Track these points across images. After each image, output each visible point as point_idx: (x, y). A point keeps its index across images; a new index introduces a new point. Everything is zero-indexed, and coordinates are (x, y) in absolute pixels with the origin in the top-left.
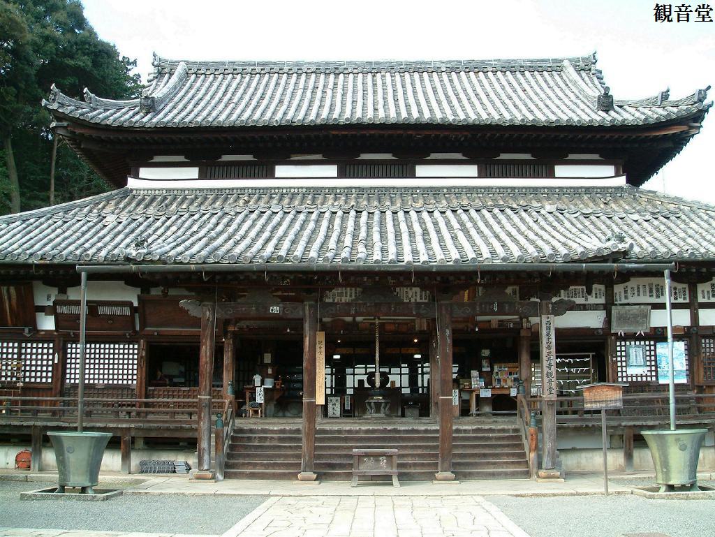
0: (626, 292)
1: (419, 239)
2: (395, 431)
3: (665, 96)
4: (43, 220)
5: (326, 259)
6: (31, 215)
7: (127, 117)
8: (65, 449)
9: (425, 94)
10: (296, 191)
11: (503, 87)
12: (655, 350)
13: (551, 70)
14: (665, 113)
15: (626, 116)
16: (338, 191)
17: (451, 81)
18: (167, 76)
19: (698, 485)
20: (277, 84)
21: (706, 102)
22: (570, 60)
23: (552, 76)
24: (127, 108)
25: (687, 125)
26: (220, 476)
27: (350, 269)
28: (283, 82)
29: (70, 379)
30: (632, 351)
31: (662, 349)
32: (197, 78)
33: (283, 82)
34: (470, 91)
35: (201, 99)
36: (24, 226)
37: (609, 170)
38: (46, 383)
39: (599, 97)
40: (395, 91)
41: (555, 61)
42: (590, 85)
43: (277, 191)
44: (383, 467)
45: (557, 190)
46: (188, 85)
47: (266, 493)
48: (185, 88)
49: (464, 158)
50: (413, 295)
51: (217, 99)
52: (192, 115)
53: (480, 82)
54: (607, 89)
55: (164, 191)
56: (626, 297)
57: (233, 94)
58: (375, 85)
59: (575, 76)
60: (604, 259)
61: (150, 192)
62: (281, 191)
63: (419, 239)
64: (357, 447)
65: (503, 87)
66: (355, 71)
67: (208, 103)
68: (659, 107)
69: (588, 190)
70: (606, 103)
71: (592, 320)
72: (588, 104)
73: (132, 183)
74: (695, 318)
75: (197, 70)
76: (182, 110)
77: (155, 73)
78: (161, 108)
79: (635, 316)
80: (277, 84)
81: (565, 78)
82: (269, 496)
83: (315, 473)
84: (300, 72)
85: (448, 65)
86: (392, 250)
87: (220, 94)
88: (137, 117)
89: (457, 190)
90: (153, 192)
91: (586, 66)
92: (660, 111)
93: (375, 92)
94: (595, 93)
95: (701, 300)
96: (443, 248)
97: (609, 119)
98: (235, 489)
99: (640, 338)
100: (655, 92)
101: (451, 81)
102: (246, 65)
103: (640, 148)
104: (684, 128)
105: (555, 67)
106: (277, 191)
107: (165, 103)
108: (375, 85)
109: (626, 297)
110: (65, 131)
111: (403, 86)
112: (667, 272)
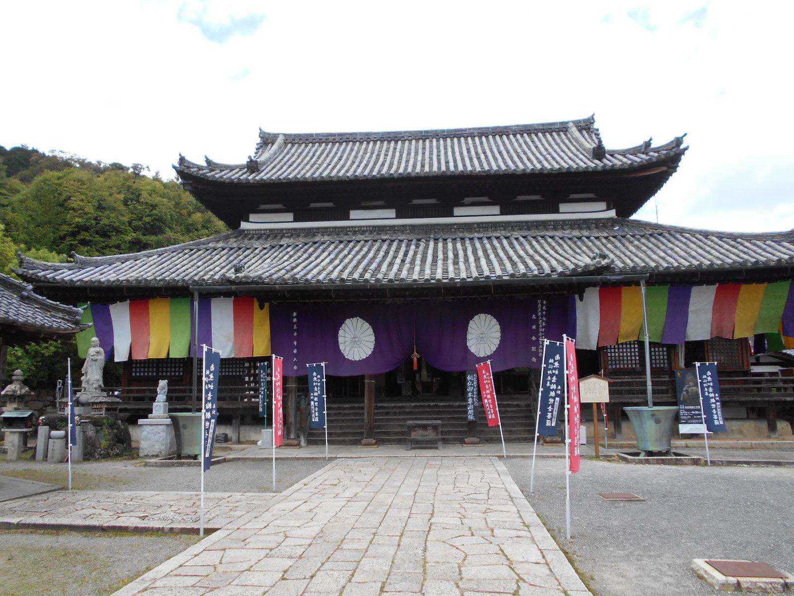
1: (450, 262)
2: (436, 406)
3: (648, 144)
4: (174, 254)
5: (378, 280)
6: (166, 250)
7: (237, 176)
8: (181, 426)
9: (461, 153)
10: (365, 229)
11: (520, 146)
13: (558, 131)
14: (648, 158)
15: (616, 162)
16: (396, 228)
17: (481, 143)
18: (270, 145)
19: (673, 451)
20: (352, 150)
21: (682, 147)
22: (574, 122)
23: (559, 135)
24: (238, 170)
26: (303, 443)
27: (394, 287)
28: (356, 148)
29: (136, 372)
32: (293, 146)
33: (356, 148)
34: (495, 150)
35: (294, 162)
36: (159, 258)
37: (603, 205)
38: (179, 376)
39: (594, 148)
40: (439, 152)
42: (589, 140)
43: (351, 229)
45: (561, 223)
46: (285, 152)
47: (334, 456)
48: (283, 154)
49: (490, 200)
51: (306, 161)
52: (286, 174)
53: (503, 143)
54: (600, 141)
55: (268, 231)
57: (319, 158)
58: (424, 148)
59: (577, 134)
60: (591, 273)
61: (257, 232)
62: (354, 229)
63: (450, 262)
64: (410, 419)
65: (520, 146)
66: (410, 138)
67: (299, 165)
68: (643, 153)
70: (599, 152)
72: (586, 155)
73: (244, 225)
75: (293, 140)
76: (279, 170)
77: (260, 143)
78: (263, 169)
80: (352, 150)
81: (569, 136)
82: (336, 458)
83: (374, 439)
84: (368, 140)
85: (480, 131)
86: (428, 271)
87: (308, 158)
88: (245, 176)
89: (484, 225)
90: (260, 232)
91: (586, 126)
92: (644, 156)
93: (424, 154)
94: (590, 145)
96: (468, 268)
97: (602, 165)
98: (312, 453)
100: (639, 142)
101: (481, 143)
102: (329, 136)
103: (631, 181)
104: (665, 168)
105: (562, 128)
106: (351, 229)
107: (267, 165)
108: (424, 148)
110: (190, 187)
111: (446, 149)
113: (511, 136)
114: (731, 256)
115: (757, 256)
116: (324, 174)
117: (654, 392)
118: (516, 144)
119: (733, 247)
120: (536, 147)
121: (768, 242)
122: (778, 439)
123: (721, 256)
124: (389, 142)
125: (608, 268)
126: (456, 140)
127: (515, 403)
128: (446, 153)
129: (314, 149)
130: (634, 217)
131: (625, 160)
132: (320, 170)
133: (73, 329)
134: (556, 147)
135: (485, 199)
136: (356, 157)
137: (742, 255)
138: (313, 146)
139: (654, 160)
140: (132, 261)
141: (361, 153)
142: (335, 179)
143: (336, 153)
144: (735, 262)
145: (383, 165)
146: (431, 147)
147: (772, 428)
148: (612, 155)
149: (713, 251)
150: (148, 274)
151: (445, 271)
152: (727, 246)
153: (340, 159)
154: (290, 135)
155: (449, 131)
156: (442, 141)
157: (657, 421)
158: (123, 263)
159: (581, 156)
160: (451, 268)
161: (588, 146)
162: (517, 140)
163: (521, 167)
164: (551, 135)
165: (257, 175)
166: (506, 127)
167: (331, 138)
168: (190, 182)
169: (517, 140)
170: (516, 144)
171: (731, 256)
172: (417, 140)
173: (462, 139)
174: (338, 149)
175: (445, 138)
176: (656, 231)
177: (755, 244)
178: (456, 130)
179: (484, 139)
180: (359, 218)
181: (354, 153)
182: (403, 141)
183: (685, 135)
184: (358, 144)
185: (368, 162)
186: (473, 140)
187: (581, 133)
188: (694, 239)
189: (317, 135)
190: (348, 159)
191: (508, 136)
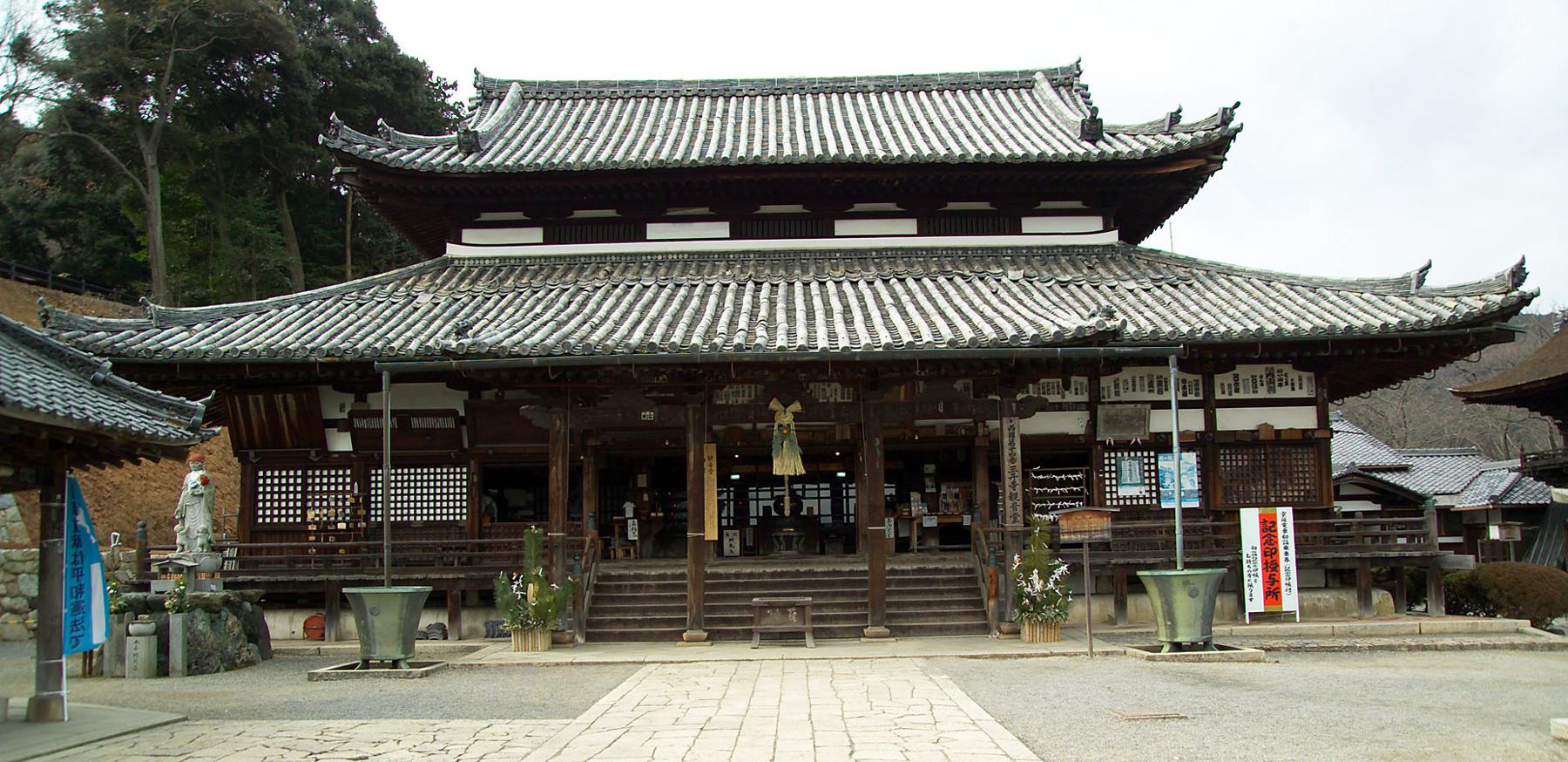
0: (1117, 386)
3: (1175, 118)
4: (329, 302)
7: (440, 159)
11: (952, 112)
12: (1156, 464)
13: (1017, 87)
14: (1174, 142)
17: (882, 104)
20: (647, 113)
21: (1232, 125)
22: (1046, 73)
25: (1205, 157)
28: (654, 110)
29: (264, 516)
30: (1125, 465)
31: (1165, 462)
32: (537, 104)
33: (654, 110)
37: (1096, 223)
40: (806, 119)
41: (1023, 73)
42: (1072, 105)
44: (793, 621)
48: (521, 120)
50: (832, 393)
51: (564, 133)
53: (921, 105)
54: (1095, 111)
56: (1271, 390)
57: (587, 127)
59: (1051, 94)
65: (952, 112)
69: (1067, 250)
70: (1093, 129)
71: (1072, 424)
73: (452, 250)
74: (1210, 420)
75: (537, 93)
79: (1130, 418)
80: (647, 113)
86: (801, 332)
87: (568, 127)
88: (455, 160)
91: (1066, 80)
95: (1219, 396)
97: (1097, 152)
99: (1136, 447)
101: (882, 104)
103: (1142, 186)
104: (1201, 162)
105: (1022, 82)
108: (778, 112)
109: (1117, 394)
112: (1172, 359)
113: (935, 94)
114: (1310, 317)
115: (1349, 318)
116: (602, 158)
117: (1186, 544)
118: (943, 109)
119: (1312, 301)
120: (981, 116)
121: (1366, 296)
122: (1375, 618)
123: (1294, 317)
124: (714, 99)
125: (1116, 334)
126: (835, 97)
127: (948, 567)
128: (819, 122)
129: (577, 110)
130: (1146, 244)
131: (1136, 145)
132: (593, 150)
133: (190, 439)
134: (1014, 116)
135: (892, 207)
136: (655, 126)
137: (1327, 316)
138: (574, 106)
139: (1186, 146)
140: (253, 315)
141: (665, 118)
142: (623, 167)
143: (619, 118)
144: (1315, 328)
145: (707, 142)
146: (791, 110)
147: (1365, 600)
148: (1113, 135)
149: (1279, 308)
150: (289, 339)
151: (832, 336)
152: (1301, 301)
153: (627, 130)
154: (533, 84)
155: (822, 81)
156: (809, 98)
157: (1193, 595)
158: (237, 318)
159: (1060, 135)
160: (840, 327)
161: (1071, 116)
162: (945, 102)
163: (957, 151)
164: (1005, 94)
165: (478, 159)
166: (925, 77)
167: (607, 92)
168: (355, 170)
169: (945, 102)
170: (943, 109)
171: (1310, 317)
172: (765, 96)
173: (847, 97)
174: (621, 111)
175: (815, 94)
176: (1184, 272)
177: (1345, 299)
178: (835, 80)
179: (885, 96)
180: (664, 237)
181: (651, 119)
182: (740, 98)
183: (1237, 105)
184: (657, 101)
185: (680, 134)
186: (867, 99)
187: (1059, 93)
188: (1248, 287)
189: (584, 83)
190: (641, 129)
191: (928, 93)
